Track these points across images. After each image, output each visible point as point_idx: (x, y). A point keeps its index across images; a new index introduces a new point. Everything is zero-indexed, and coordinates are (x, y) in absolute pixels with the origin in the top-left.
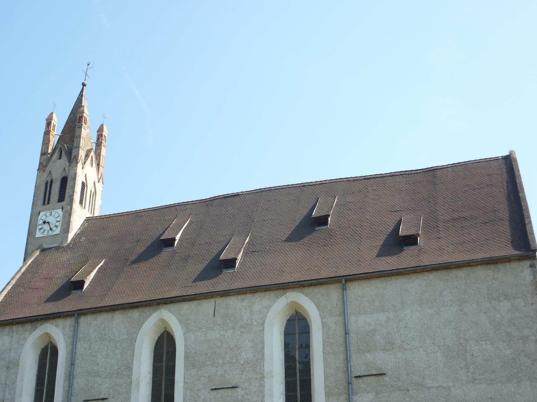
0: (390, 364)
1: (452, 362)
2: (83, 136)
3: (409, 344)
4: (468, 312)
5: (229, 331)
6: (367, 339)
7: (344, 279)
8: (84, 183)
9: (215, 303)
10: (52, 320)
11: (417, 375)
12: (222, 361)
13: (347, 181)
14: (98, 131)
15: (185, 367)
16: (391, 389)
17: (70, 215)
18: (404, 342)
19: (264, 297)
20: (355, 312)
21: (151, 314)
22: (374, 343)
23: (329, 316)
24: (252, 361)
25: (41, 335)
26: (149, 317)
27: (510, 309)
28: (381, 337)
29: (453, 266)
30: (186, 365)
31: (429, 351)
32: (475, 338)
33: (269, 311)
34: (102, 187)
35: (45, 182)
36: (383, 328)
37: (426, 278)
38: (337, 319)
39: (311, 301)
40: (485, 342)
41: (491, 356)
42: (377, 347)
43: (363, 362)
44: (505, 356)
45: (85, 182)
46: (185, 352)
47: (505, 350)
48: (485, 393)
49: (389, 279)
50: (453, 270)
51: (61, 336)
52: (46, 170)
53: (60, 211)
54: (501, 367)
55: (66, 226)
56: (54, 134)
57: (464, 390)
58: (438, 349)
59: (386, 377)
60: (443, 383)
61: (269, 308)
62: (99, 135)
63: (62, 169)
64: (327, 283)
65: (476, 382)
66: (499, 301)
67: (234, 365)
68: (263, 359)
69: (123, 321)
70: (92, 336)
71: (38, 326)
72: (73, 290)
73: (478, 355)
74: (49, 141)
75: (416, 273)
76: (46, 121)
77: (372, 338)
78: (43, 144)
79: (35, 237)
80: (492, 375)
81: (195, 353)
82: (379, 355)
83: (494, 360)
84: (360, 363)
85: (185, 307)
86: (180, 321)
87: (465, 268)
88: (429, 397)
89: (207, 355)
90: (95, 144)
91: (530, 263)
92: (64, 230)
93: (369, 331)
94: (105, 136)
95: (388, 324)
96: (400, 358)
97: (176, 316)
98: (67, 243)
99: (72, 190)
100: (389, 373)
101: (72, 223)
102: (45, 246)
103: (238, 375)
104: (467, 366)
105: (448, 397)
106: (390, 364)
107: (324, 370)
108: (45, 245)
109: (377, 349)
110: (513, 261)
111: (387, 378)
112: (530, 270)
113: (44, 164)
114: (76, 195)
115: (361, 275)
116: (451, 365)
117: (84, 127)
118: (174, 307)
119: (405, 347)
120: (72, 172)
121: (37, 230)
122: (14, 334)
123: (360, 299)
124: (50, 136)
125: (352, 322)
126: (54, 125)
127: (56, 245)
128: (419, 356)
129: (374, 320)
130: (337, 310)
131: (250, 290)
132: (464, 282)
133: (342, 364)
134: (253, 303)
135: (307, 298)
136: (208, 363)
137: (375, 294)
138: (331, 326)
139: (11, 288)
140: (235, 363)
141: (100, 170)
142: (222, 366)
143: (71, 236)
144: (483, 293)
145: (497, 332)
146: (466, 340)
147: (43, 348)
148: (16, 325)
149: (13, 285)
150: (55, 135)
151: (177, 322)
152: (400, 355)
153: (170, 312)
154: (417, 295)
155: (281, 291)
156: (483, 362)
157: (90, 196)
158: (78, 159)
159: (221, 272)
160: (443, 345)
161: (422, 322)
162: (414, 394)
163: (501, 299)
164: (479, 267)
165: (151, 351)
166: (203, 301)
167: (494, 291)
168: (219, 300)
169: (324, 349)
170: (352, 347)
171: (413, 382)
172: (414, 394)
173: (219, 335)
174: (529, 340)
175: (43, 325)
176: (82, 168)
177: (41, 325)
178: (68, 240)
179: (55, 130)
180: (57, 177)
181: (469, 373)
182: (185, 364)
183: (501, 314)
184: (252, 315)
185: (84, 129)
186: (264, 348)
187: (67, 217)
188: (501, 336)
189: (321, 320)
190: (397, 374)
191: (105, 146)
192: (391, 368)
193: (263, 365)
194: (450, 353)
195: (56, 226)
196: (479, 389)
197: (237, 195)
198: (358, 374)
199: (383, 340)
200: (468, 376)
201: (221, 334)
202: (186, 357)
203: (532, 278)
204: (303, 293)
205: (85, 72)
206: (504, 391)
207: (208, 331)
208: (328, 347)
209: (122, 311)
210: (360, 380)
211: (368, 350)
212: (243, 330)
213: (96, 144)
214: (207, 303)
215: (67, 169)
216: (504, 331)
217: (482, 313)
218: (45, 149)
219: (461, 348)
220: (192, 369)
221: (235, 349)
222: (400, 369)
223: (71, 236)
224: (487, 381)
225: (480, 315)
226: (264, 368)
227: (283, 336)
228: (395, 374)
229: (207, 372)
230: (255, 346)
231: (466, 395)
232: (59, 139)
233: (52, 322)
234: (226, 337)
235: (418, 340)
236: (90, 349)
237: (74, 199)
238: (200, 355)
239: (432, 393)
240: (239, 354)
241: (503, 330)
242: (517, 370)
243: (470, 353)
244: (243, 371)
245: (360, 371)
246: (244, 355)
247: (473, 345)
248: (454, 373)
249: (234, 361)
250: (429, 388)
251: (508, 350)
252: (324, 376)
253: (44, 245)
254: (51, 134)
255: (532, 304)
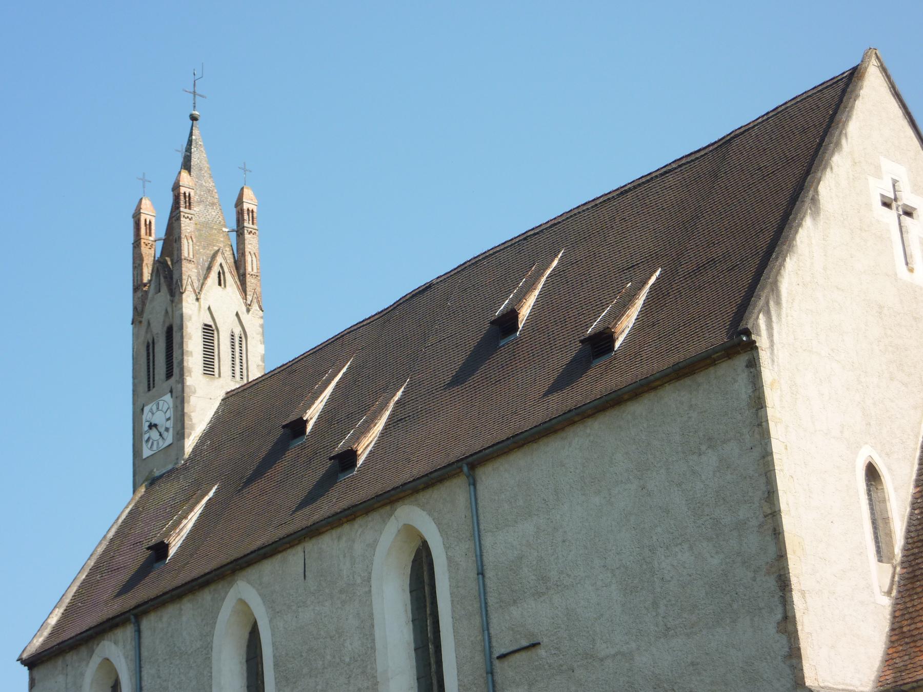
0: (545, 622)
1: (633, 599)
2: (187, 234)
3: (569, 576)
4: (652, 489)
5: (327, 604)
6: (510, 577)
7: (464, 465)
8: (210, 326)
9: (304, 552)
10: (109, 633)
11: (585, 636)
12: (321, 663)
13: (592, 207)
14: (236, 206)
15: (276, 684)
16: (548, 673)
17: (182, 401)
18: (562, 572)
19: (367, 526)
20: (492, 526)
21: (227, 593)
22: (521, 583)
23: (456, 543)
24: (359, 656)
25: (100, 664)
26: (224, 599)
27: (718, 467)
28: (530, 570)
29: (626, 397)
30: (277, 680)
31: (599, 583)
32: (665, 541)
33: (374, 552)
34: (262, 317)
35: (146, 344)
36: (532, 550)
37: (588, 431)
38: (467, 547)
39: (431, 518)
40: (679, 546)
41: (690, 576)
42: (526, 590)
43: (507, 626)
44: (711, 571)
45: (211, 323)
46: (274, 656)
47: (712, 557)
48: (684, 654)
49: (535, 446)
50: (629, 403)
51: (123, 660)
52: (143, 320)
53: (168, 397)
54: (707, 594)
55: (179, 425)
56: (150, 242)
57: (653, 655)
58: (612, 577)
59: (541, 649)
60: (622, 646)
61: (373, 546)
62: (239, 212)
63: (163, 312)
64: (448, 477)
65: (670, 633)
66: (700, 455)
67: (338, 668)
68: (373, 648)
69: (193, 615)
70: (160, 652)
71: (95, 647)
72: (156, 563)
73: (671, 577)
74: (142, 260)
75: (572, 424)
76: (132, 219)
77: (517, 575)
78: (134, 268)
79: (142, 457)
80: (694, 615)
81: (287, 654)
82: (530, 606)
83: (695, 582)
84: (503, 628)
85: (268, 568)
86: (263, 596)
87: (647, 395)
88: (604, 678)
89: (302, 656)
90: (235, 233)
91: (747, 358)
92: (177, 434)
93: (513, 562)
94: (251, 209)
95: (539, 541)
96: (558, 606)
97: (257, 590)
98: (183, 460)
99: (180, 351)
100: (545, 641)
101: (190, 416)
102: (157, 473)
103: (344, 685)
104: (655, 604)
105: (630, 674)
106: (545, 622)
107: (456, 652)
108: (157, 470)
109: (526, 595)
110: (718, 362)
111: (541, 652)
112: (746, 374)
113: (139, 309)
114: (190, 358)
115: (487, 451)
116: (632, 605)
117: (186, 215)
118: (253, 572)
119: (565, 582)
120: (177, 314)
121: (144, 443)
122: (69, 668)
123: (497, 498)
124: (142, 248)
125: (488, 547)
126: (148, 223)
127: (170, 467)
128: (585, 597)
129: (519, 536)
130: (466, 527)
131: (346, 517)
132: (645, 425)
133: (479, 636)
134: (354, 541)
135: (424, 513)
136: (304, 671)
137: (517, 483)
138: (461, 561)
139: (86, 576)
140: (338, 664)
141: (248, 284)
142: (323, 673)
143: (189, 444)
144: (675, 442)
145: (698, 521)
146: (653, 550)
147: (112, 685)
148: (69, 652)
149: (90, 570)
150: (154, 243)
151: (259, 600)
152: (558, 601)
153: (249, 584)
154: (577, 471)
155: (388, 508)
156: (679, 589)
157: (233, 345)
158: (182, 286)
159: (337, 478)
160: (618, 566)
161: (587, 524)
162: (582, 677)
163: (703, 448)
164: (668, 388)
165: (241, 662)
166: (289, 551)
167: (691, 434)
168: (310, 546)
169: (453, 611)
170: (491, 598)
171: (579, 652)
172: (582, 677)
173: (314, 613)
174: (747, 529)
175: (100, 645)
176: (194, 301)
177: (98, 645)
178: (186, 453)
179: (153, 231)
180: (159, 330)
181: (658, 618)
182: (276, 679)
183: (703, 482)
184: (354, 564)
185: (188, 219)
186: (373, 626)
187: (179, 406)
188: (704, 530)
189: (445, 554)
190: (556, 639)
191: (253, 231)
192: (547, 630)
193: (375, 660)
194: (630, 581)
195: (167, 430)
196: (675, 649)
197: (428, 287)
198: (503, 651)
199: (534, 574)
200: (657, 625)
201: (316, 611)
202: (276, 665)
203: (750, 391)
204: (419, 505)
205: (190, 92)
206: (712, 644)
207: (300, 610)
208: (458, 606)
209: (190, 597)
210: (506, 663)
211: (514, 600)
212: (344, 597)
213: (237, 232)
214: (294, 555)
215: (170, 310)
216: (708, 517)
217: (675, 486)
218: (137, 277)
219: (645, 567)
220: (285, 686)
221: (337, 636)
222: (560, 629)
223: (189, 444)
224: (686, 629)
225: (672, 491)
226: (376, 665)
227: (409, 594)
228: (554, 640)
229: (667, 607)
230: (362, 624)
231: (656, 663)
232: (163, 248)
233: (109, 636)
234: (323, 615)
235: (583, 564)
236: (159, 677)
237: (185, 368)
238: (293, 657)
239: (607, 670)
240: (343, 645)
241: (708, 515)
242: (731, 596)
243: (658, 576)
244: (350, 677)
245: (505, 644)
246: (349, 646)
247: (663, 557)
248: (637, 621)
249: (338, 660)
250: (602, 660)
251: (716, 557)
252: (456, 664)
253: (155, 470)
254: (142, 243)
255: (752, 448)
